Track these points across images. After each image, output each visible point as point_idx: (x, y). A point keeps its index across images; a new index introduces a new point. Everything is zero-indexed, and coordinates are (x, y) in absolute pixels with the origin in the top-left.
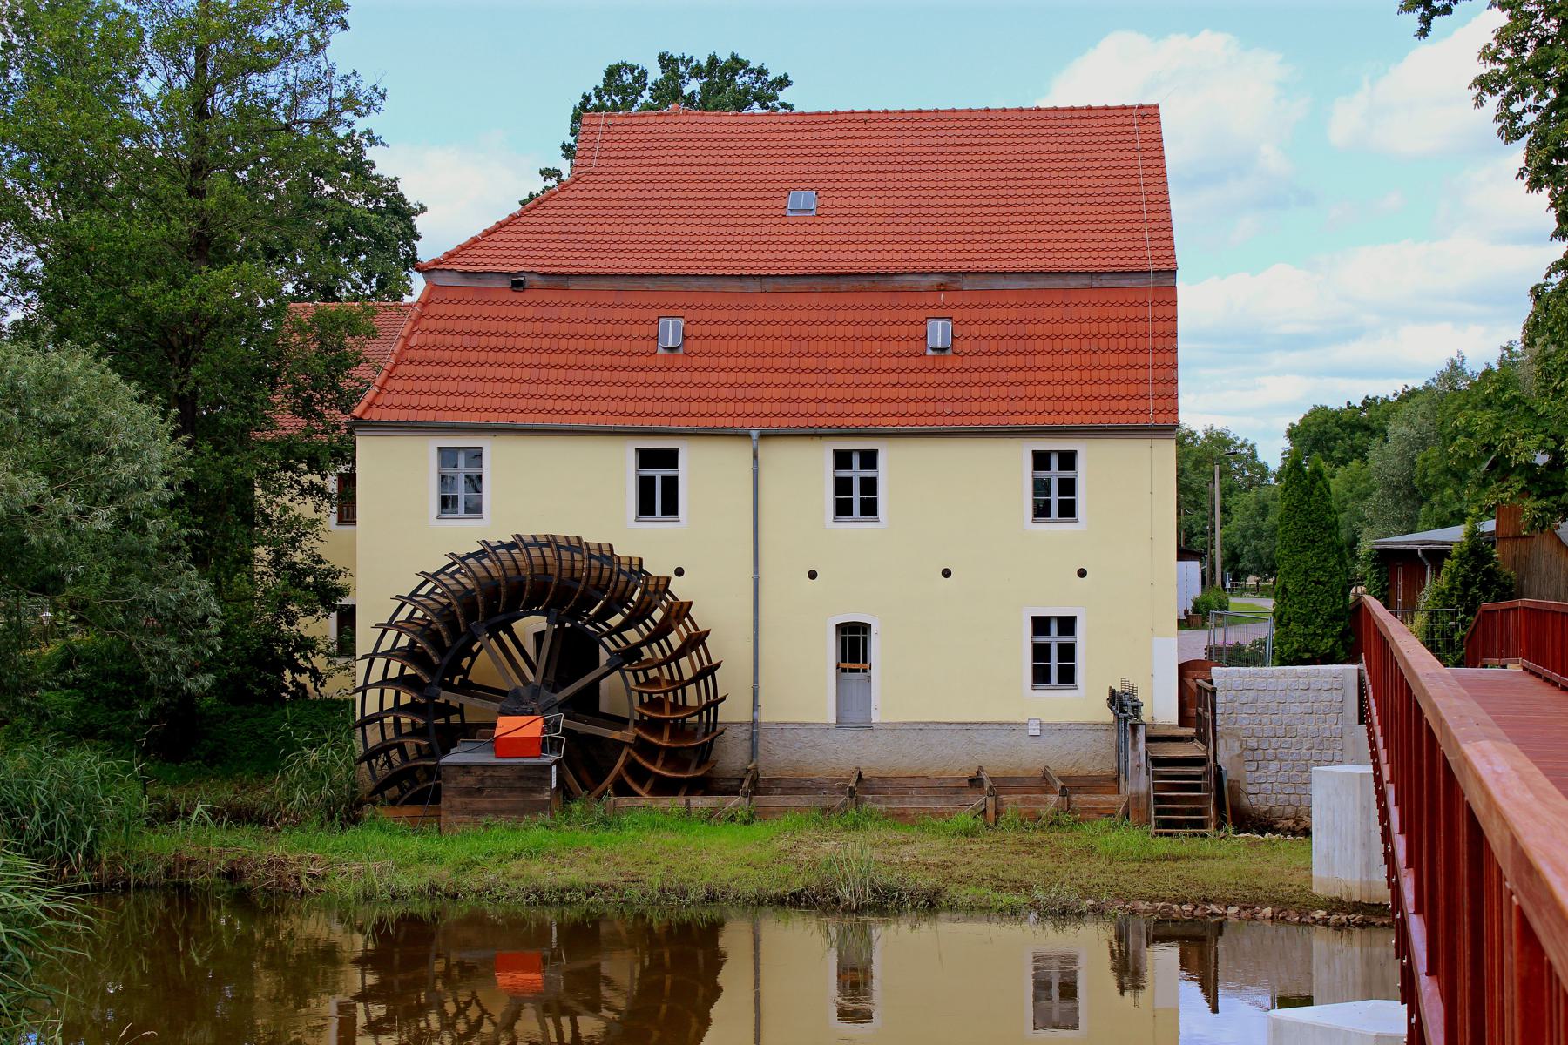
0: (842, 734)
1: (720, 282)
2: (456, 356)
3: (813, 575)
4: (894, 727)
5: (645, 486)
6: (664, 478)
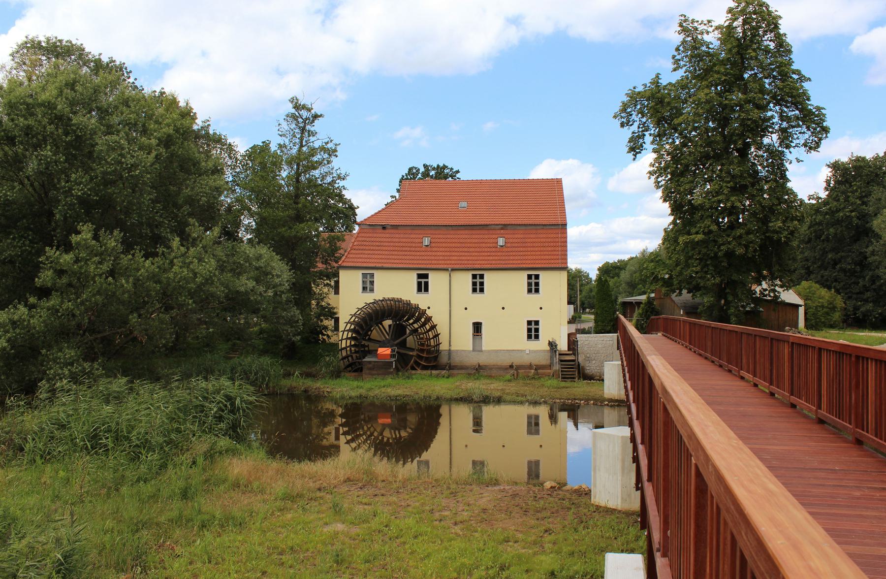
2: (367, 248)
4: (489, 351)
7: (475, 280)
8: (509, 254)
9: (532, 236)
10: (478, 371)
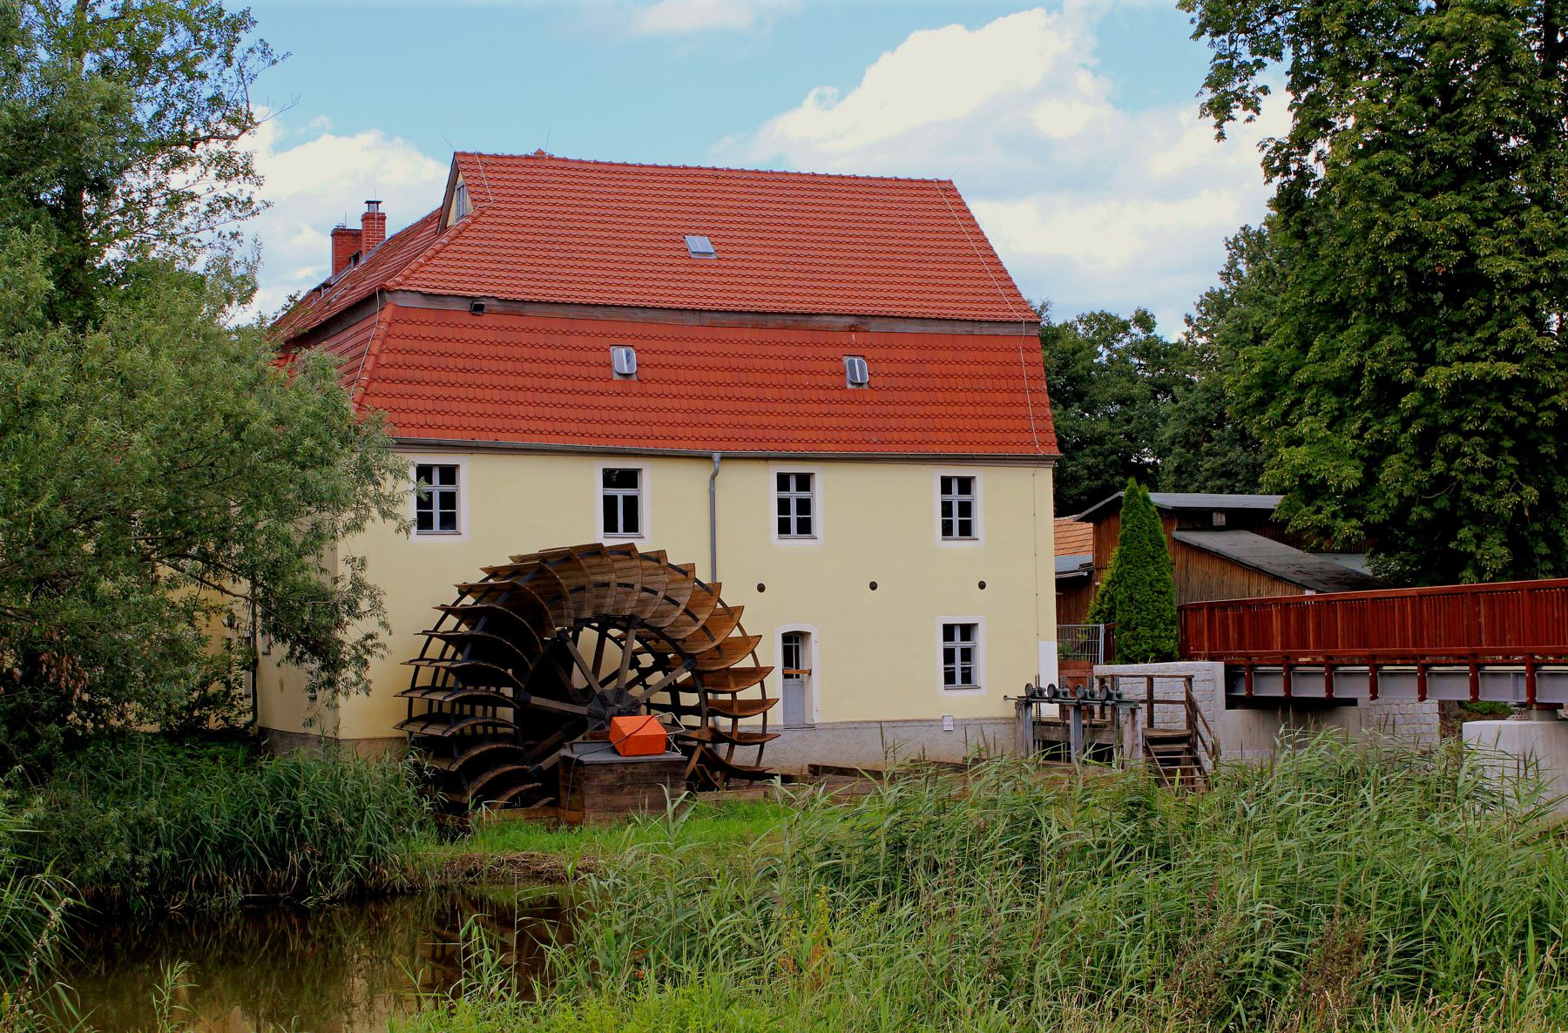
1: (663, 314)
3: (761, 588)
4: (833, 727)
5: (609, 503)
6: (625, 498)
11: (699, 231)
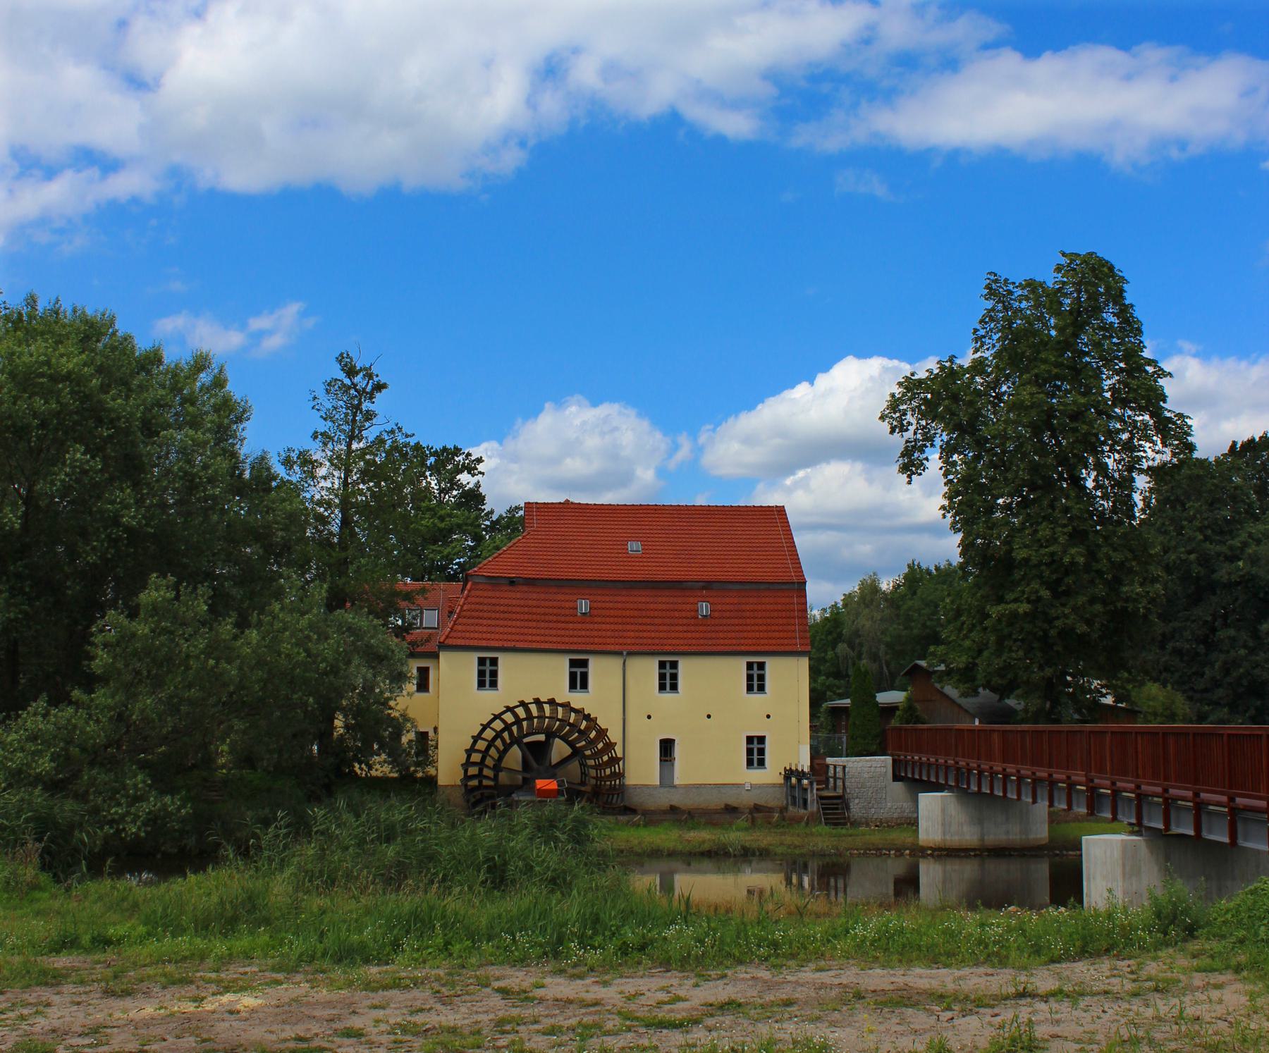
0: (662, 790)
2: (486, 615)
7: (663, 671)
8: (717, 628)
9: (751, 600)
10: (676, 815)
11: (637, 539)
